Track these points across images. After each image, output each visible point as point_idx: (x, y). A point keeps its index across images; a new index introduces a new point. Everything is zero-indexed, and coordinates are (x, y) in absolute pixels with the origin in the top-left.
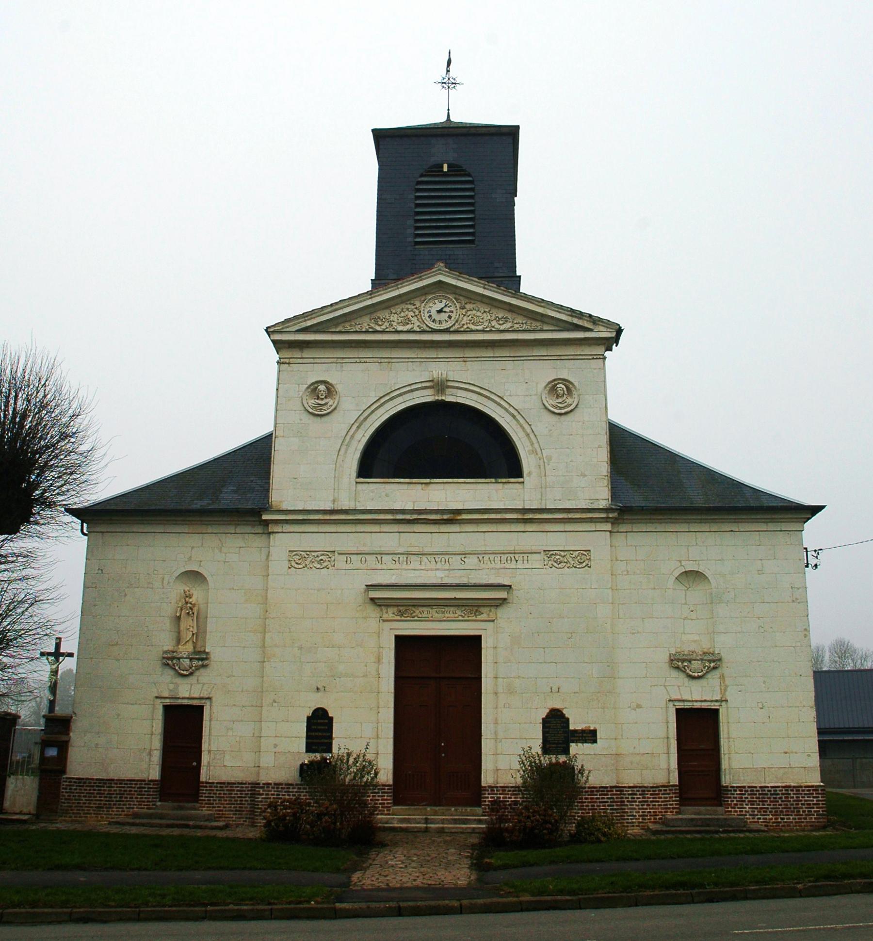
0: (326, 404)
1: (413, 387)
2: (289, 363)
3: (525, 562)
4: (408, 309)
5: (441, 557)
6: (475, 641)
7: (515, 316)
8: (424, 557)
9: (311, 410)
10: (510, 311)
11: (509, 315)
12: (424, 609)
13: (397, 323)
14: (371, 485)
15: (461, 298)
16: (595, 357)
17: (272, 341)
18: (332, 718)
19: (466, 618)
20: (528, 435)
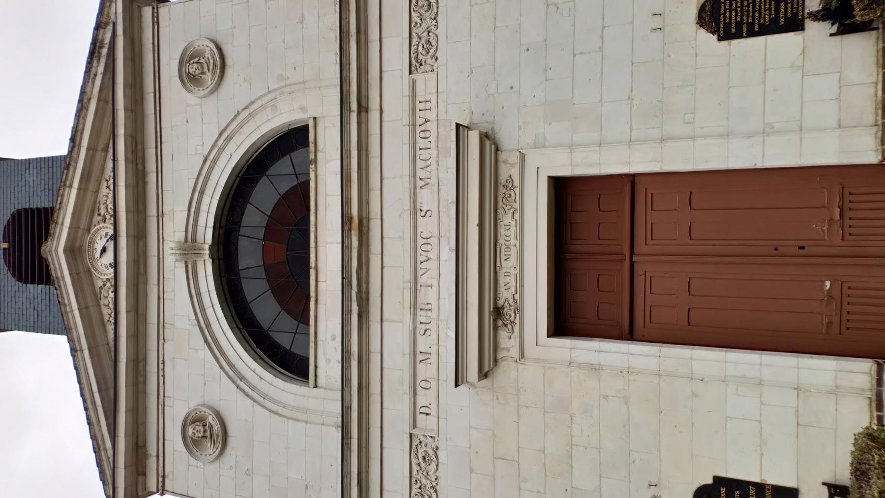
3: (428, 105)
5: (419, 251)
6: (563, 190)
8: (422, 280)
12: (502, 280)
14: (320, 364)
18: (717, 479)
19: (517, 205)
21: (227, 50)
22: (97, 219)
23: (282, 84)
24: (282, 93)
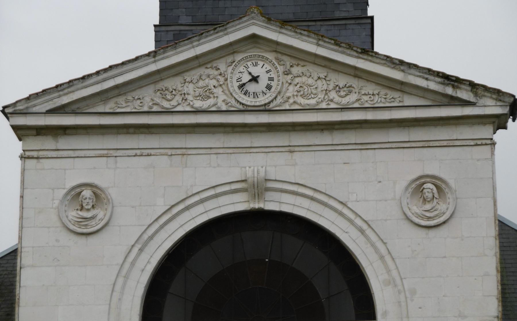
0: (93, 218)
1: (219, 190)
2: (38, 158)
4: (209, 76)
7: (362, 83)
9: (72, 227)
10: (355, 76)
11: (354, 82)
13: (190, 95)
15: (284, 58)
16: (479, 143)
17: (16, 128)
20: (382, 258)
21: (443, 231)
22: (288, 61)
23: (408, 295)
24: (399, 292)
